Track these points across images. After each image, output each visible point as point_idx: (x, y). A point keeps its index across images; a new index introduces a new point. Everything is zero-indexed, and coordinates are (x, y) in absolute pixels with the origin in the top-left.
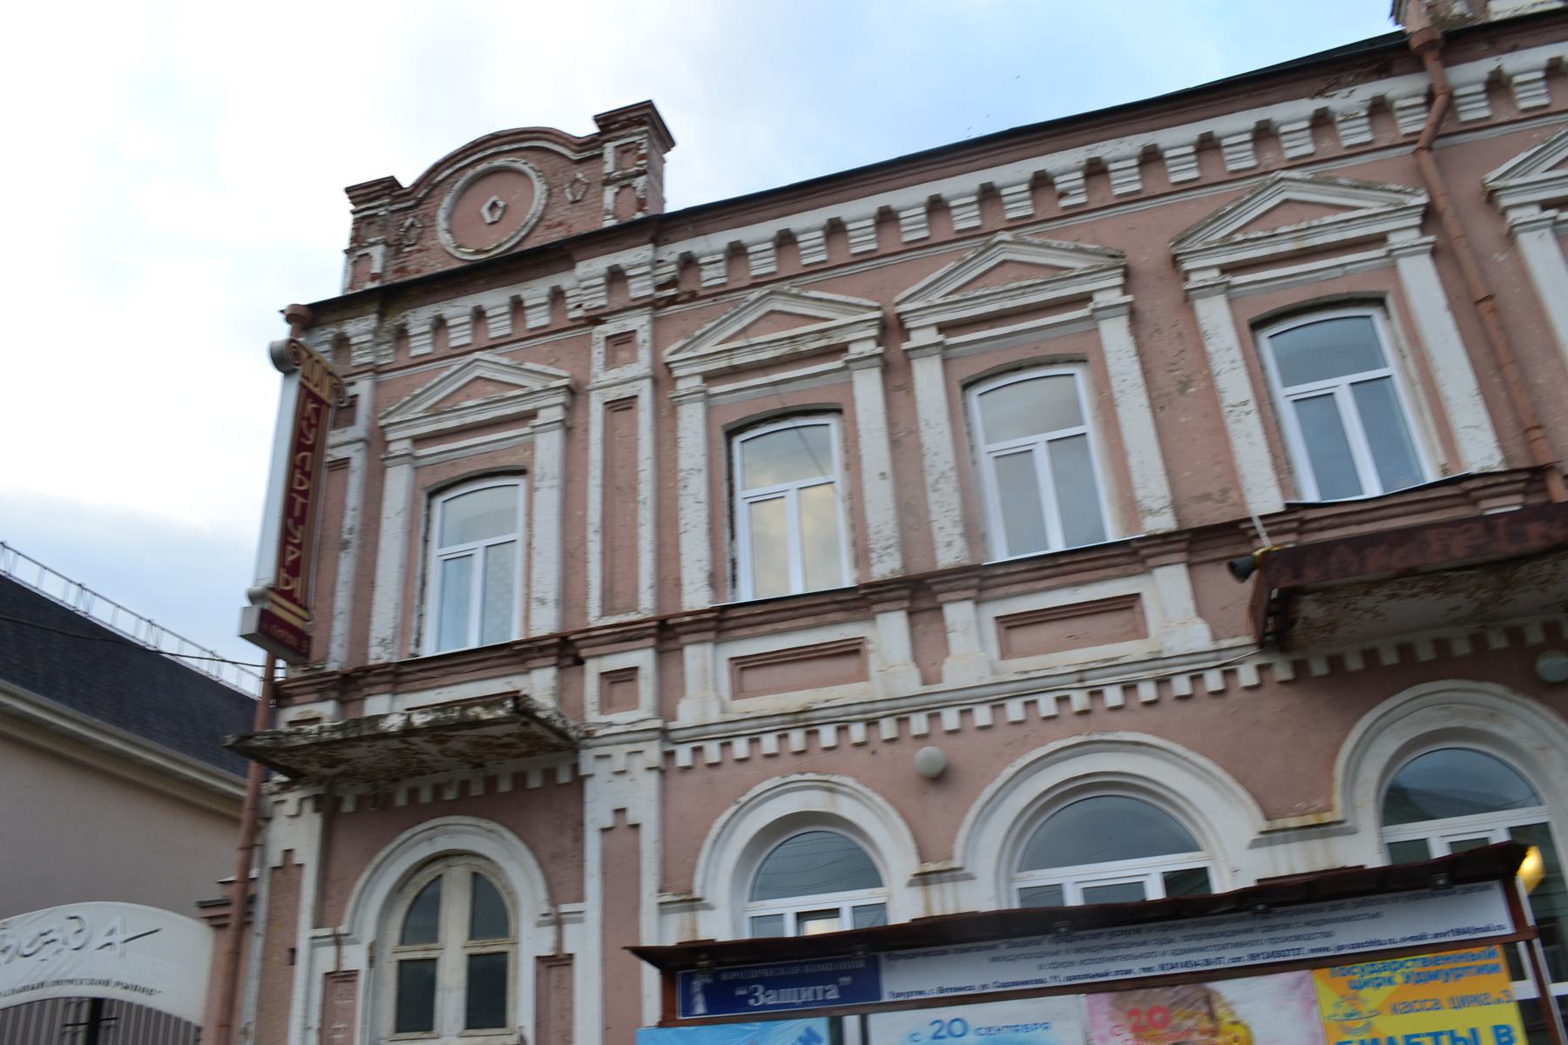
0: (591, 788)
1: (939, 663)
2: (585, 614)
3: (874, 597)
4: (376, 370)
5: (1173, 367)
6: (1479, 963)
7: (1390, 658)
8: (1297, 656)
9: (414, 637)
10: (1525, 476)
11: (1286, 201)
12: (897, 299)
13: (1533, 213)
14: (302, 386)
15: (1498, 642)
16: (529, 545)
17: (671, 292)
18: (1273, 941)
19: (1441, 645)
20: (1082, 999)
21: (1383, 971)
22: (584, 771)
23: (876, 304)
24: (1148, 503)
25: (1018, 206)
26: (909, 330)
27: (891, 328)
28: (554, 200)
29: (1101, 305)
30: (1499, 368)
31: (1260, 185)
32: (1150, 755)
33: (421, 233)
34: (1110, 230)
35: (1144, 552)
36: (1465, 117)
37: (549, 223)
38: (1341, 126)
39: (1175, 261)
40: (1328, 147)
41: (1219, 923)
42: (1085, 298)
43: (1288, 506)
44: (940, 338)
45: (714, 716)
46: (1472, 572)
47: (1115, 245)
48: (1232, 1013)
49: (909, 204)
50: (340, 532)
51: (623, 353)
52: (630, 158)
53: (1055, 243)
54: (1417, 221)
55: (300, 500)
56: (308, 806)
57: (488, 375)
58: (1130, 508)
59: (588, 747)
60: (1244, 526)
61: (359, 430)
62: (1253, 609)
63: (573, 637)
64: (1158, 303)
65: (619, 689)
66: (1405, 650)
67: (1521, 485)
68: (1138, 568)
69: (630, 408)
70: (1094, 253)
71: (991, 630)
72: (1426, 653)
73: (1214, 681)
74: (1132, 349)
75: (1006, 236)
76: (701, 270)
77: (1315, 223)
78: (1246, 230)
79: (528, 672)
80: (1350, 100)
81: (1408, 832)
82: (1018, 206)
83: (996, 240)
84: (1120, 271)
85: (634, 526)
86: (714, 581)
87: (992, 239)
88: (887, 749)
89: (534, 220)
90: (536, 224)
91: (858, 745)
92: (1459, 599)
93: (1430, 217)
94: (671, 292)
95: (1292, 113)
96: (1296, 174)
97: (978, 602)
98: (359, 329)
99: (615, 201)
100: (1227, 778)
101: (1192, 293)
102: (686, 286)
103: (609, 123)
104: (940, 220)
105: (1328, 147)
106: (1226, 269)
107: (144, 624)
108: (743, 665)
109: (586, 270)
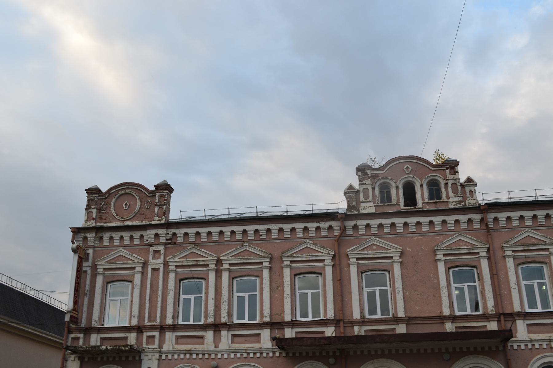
0: (143, 362)
1: (219, 343)
2: (144, 321)
3: (207, 327)
4: (94, 247)
5: (276, 283)
7: (304, 354)
9: (103, 320)
12: (221, 256)
14: (79, 256)
15: (324, 354)
16: (132, 301)
17: (170, 241)
22: (142, 358)
23: (216, 256)
26: (223, 263)
27: (219, 262)
28: (142, 206)
29: (264, 266)
33: (106, 208)
35: (262, 326)
36: (347, 233)
37: (140, 213)
39: (281, 258)
42: (261, 263)
43: (292, 320)
44: (229, 267)
45: (171, 349)
49: (227, 231)
50: (85, 291)
51: (157, 255)
52: (162, 199)
54: (331, 258)
55: (77, 285)
56: (77, 359)
57: (123, 255)
59: (143, 353)
61: (89, 263)
63: (141, 327)
65: (151, 340)
67: (335, 323)
68: (261, 328)
69: (158, 270)
70: (265, 252)
71: (230, 337)
74: (269, 277)
76: (177, 237)
77: (311, 255)
79: (130, 333)
85: (157, 301)
86: (174, 317)
88: (206, 360)
89: (137, 212)
90: (137, 213)
91: (200, 359)
94: (170, 241)
95: (312, 225)
97: (228, 331)
98: (91, 236)
99: (158, 211)
102: (173, 241)
103: (157, 187)
106: (291, 262)
107: (8, 278)
108: (178, 337)
109: (149, 232)
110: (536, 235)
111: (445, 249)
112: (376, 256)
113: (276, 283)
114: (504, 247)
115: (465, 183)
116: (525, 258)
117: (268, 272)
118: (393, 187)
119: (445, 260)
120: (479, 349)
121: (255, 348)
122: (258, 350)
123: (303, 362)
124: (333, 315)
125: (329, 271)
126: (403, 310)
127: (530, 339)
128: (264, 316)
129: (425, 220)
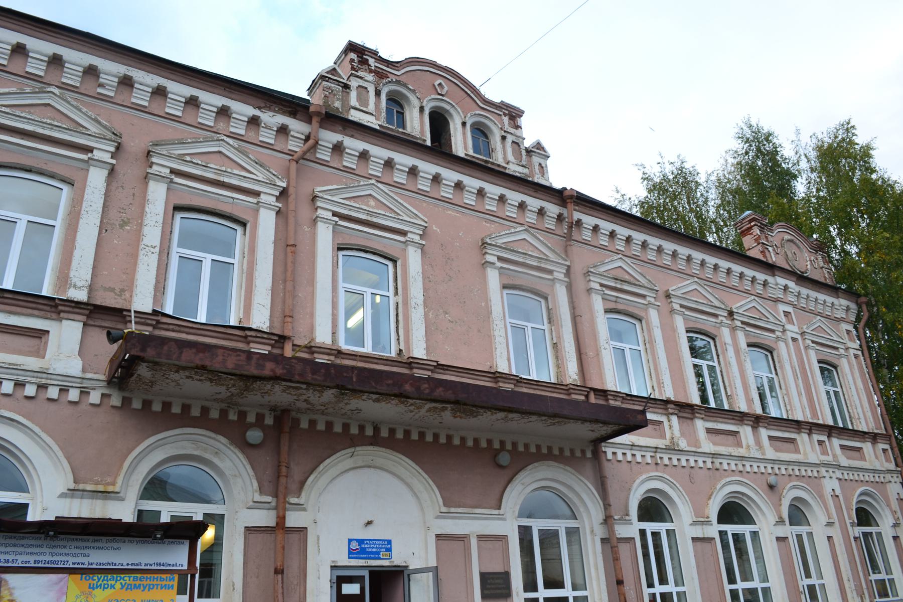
5: (122, 211)
6: (164, 583)
7: (176, 409)
8: (127, 394)
10: (276, 338)
11: (220, 152)
13: (329, 215)
15: (233, 416)
18: (52, 554)
19: (205, 410)
20: (411, 582)
21: (110, 579)
24: (74, 280)
25: (71, 77)
29: (95, 158)
30: (285, 281)
31: (210, 137)
32: (20, 430)
34: (120, 119)
35: (60, 308)
36: (318, 156)
38: (262, 129)
40: (251, 136)
41: (23, 538)
42: (89, 150)
43: (154, 310)
46: (233, 377)
47: (118, 129)
48: (11, 594)
53: (84, 110)
54: (277, 194)
58: (63, 279)
60: (125, 313)
62: (112, 361)
64: (129, 172)
66: (186, 408)
68: (54, 316)
70: (105, 127)
72: (196, 412)
73: (74, 395)
74: (103, 190)
75: (56, 91)
77: (229, 170)
78: (193, 156)
80: (272, 119)
81: (151, 505)
82: (71, 77)
83: (49, 89)
84: (116, 144)
87: (45, 88)
92: (222, 389)
93: (283, 194)
95: (242, 110)
96: (230, 141)
100: (60, 454)
101: (150, 175)
104: (19, 60)
105: (251, 136)
106: (173, 171)
110: (632, 270)
111: (503, 246)
112: (375, 220)
113: (120, 212)
114: (590, 274)
115: (533, 148)
116: (616, 302)
117: (104, 179)
118: (414, 107)
119: (502, 268)
120: (556, 452)
121: (22, 367)
122: (33, 377)
123: (175, 428)
124: (268, 324)
125: (267, 222)
126: (425, 346)
127: (631, 444)
128: (71, 284)
129: (450, 175)
